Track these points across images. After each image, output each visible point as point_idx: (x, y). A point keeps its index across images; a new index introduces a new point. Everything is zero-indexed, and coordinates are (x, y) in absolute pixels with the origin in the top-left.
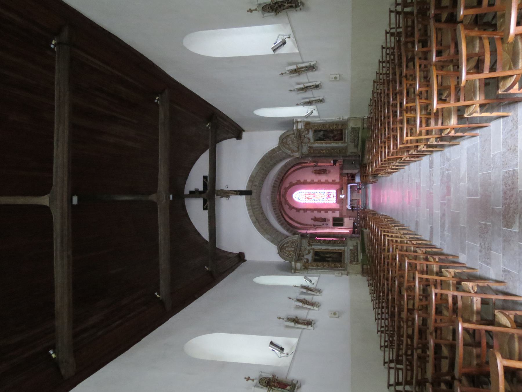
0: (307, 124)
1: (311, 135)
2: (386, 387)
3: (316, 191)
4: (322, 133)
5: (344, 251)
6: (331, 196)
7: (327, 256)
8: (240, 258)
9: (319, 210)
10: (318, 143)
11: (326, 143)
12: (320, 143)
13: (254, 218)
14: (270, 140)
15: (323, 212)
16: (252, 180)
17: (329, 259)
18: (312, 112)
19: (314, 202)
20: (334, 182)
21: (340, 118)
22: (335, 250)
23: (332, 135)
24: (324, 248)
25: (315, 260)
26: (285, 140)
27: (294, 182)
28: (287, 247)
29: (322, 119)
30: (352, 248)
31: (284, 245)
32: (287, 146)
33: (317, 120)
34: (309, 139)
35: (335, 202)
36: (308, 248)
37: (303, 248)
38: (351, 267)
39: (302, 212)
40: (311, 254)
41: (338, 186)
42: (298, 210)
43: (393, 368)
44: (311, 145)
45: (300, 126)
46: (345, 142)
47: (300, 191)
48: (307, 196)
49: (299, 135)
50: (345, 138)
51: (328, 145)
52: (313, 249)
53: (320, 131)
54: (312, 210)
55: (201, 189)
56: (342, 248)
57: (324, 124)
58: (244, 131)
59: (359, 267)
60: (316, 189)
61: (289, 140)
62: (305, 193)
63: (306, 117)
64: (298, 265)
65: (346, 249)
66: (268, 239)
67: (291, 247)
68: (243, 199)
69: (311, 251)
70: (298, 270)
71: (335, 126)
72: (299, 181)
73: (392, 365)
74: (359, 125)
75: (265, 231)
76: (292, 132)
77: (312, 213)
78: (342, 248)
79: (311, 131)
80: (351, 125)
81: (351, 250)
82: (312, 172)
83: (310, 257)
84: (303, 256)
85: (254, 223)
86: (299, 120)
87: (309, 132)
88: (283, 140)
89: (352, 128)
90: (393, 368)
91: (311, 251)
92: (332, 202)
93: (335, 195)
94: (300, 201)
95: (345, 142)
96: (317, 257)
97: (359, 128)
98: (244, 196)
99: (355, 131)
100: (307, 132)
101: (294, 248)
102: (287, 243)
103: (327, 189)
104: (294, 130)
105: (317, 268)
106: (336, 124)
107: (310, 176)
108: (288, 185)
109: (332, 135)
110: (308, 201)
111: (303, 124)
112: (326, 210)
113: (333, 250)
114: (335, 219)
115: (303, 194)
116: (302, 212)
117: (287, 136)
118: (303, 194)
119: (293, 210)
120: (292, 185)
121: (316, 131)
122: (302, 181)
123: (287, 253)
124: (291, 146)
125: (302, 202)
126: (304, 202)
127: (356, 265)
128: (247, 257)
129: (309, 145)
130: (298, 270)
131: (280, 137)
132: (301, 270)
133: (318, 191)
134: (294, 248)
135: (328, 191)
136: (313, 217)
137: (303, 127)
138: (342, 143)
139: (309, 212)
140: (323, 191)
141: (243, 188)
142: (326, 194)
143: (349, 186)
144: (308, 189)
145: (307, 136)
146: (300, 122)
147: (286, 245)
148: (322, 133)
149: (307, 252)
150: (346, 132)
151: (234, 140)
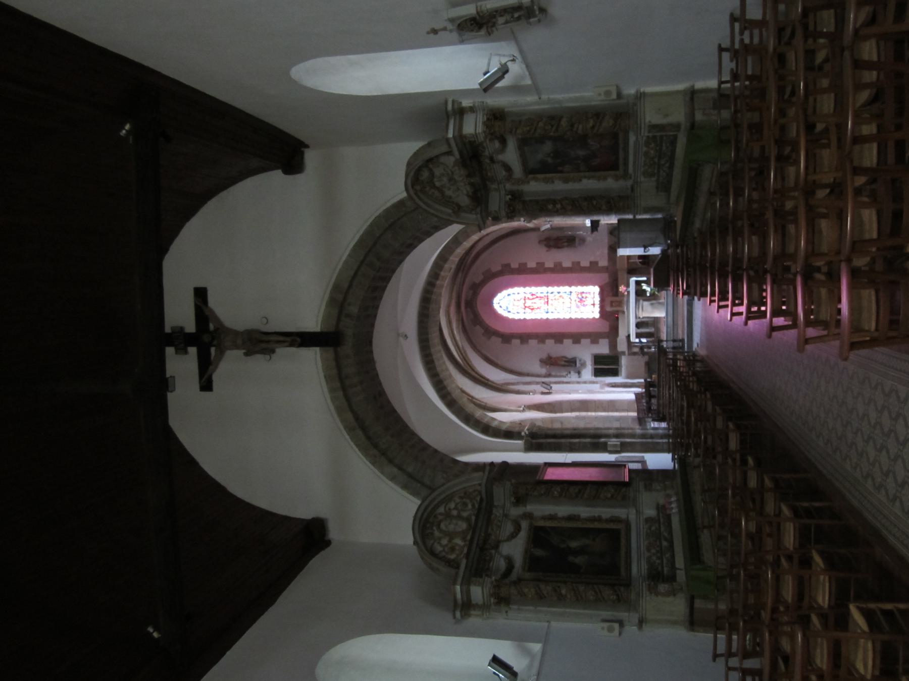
0: (496, 116)
1: (511, 155)
2: (711, 658)
3: (550, 289)
4: (548, 147)
5: (627, 523)
6: (589, 301)
7: (574, 544)
8: (312, 537)
9: (559, 337)
10: (536, 180)
11: (566, 181)
12: (546, 181)
13: (350, 416)
14: (380, 177)
15: (568, 342)
16: (339, 300)
17: (579, 560)
18: (504, 71)
19: (545, 316)
20: (593, 267)
21: (608, 93)
22: (599, 519)
23: (581, 153)
24: (563, 510)
25: (532, 563)
26: (425, 174)
27: (496, 268)
28: (448, 515)
29: (545, 97)
30: (651, 512)
31: (437, 506)
32: (437, 193)
33: (528, 102)
34: (508, 168)
35: (597, 316)
36: (515, 512)
37: (497, 512)
38: (651, 604)
39: (516, 342)
40: (523, 534)
41: (605, 277)
42: (507, 338)
43: (734, 669)
44: (515, 188)
45: (472, 126)
46: (626, 175)
47: (510, 291)
48: (529, 303)
49: (472, 155)
50: (626, 164)
51: (570, 186)
52: (529, 516)
53: (541, 140)
54: (542, 337)
55: (190, 327)
56: (620, 512)
57: (553, 118)
58: (307, 146)
59: (678, 606)
60: (548, 285)
61: (438, 171)
62: (522, 296)
63: (487, 87)
64: (477, 593)
65: (632, 517)
66: (393, 478)
67: (459, 517)
68: (312, 357)
69: (524, 525)
70: (476, 606)
71: (591, 123)
72: (508, 265)
73: (734, 662)
74: (678, 115)
75: (384, 453)
76: (444, 148)
77: (541, 345)
78: (620, 512)
79: (512, 144)
80: (650, 116)
81: (648, 520)
82: (540, 242)
83: (515, 549)
84: (496, 547)
85: (350, 430)
86: (466, 103)
87: (503, 142)
88: (420, 174)
89: (653, 127)
90: (734, 669)
91: (524, 525)
92: (591, 316)
93: (597, 299)
94: (510, 316)
95: (626, 175)
96: (539, 552)
97: (677, 127)
98: (317, 349)
99: (662, 136)
100: (497, 144)
101: (467, 520)
102: (449, 499)
103: (576, 285)
104: (447, 140)
105: (541, 598)
106: (598, 114)
107: (535, 254)
108: (481, 277)
109: (581, 153)
110: (530, 316)
111: (481, 118)
112: (577, 338)
113: (593, 519)
114: (598, 359)
115: (517, 297)
116: (516, 342)
117: (430, 160)
118: (517, 297)
119: (494, 339)
120: (490, 276)
121: (523, 143)
122: (515, 265)
123: (445, 541)
124: (448, 193)
125: (517, 317)
126: (521, 316)
127: (671, 599)
128: (334, 533)
129: (508, 186)
130: (476, 606)
131: (409, 164)
132: (484, 608)
133: (556, 289)
134: (467, 520)
135: (580, 289)
136: (544, 356)
137: (480, 129)
138: (617, 178)
139: (533, 342)
140: (567, 289)
141: (312, 322)
142: (574, 296)
143: (633, 280)
144: (530, 286)
145: (501, 157)
146: (472, 109)
147: (441, 510)
148: (548, 147)
149: (509, 528)
150: (632, 138)
151: (277, 176)
